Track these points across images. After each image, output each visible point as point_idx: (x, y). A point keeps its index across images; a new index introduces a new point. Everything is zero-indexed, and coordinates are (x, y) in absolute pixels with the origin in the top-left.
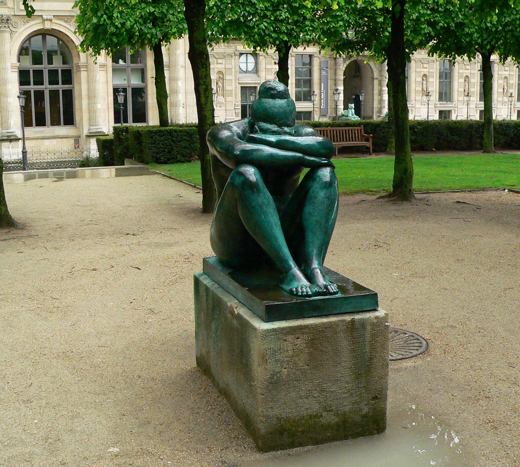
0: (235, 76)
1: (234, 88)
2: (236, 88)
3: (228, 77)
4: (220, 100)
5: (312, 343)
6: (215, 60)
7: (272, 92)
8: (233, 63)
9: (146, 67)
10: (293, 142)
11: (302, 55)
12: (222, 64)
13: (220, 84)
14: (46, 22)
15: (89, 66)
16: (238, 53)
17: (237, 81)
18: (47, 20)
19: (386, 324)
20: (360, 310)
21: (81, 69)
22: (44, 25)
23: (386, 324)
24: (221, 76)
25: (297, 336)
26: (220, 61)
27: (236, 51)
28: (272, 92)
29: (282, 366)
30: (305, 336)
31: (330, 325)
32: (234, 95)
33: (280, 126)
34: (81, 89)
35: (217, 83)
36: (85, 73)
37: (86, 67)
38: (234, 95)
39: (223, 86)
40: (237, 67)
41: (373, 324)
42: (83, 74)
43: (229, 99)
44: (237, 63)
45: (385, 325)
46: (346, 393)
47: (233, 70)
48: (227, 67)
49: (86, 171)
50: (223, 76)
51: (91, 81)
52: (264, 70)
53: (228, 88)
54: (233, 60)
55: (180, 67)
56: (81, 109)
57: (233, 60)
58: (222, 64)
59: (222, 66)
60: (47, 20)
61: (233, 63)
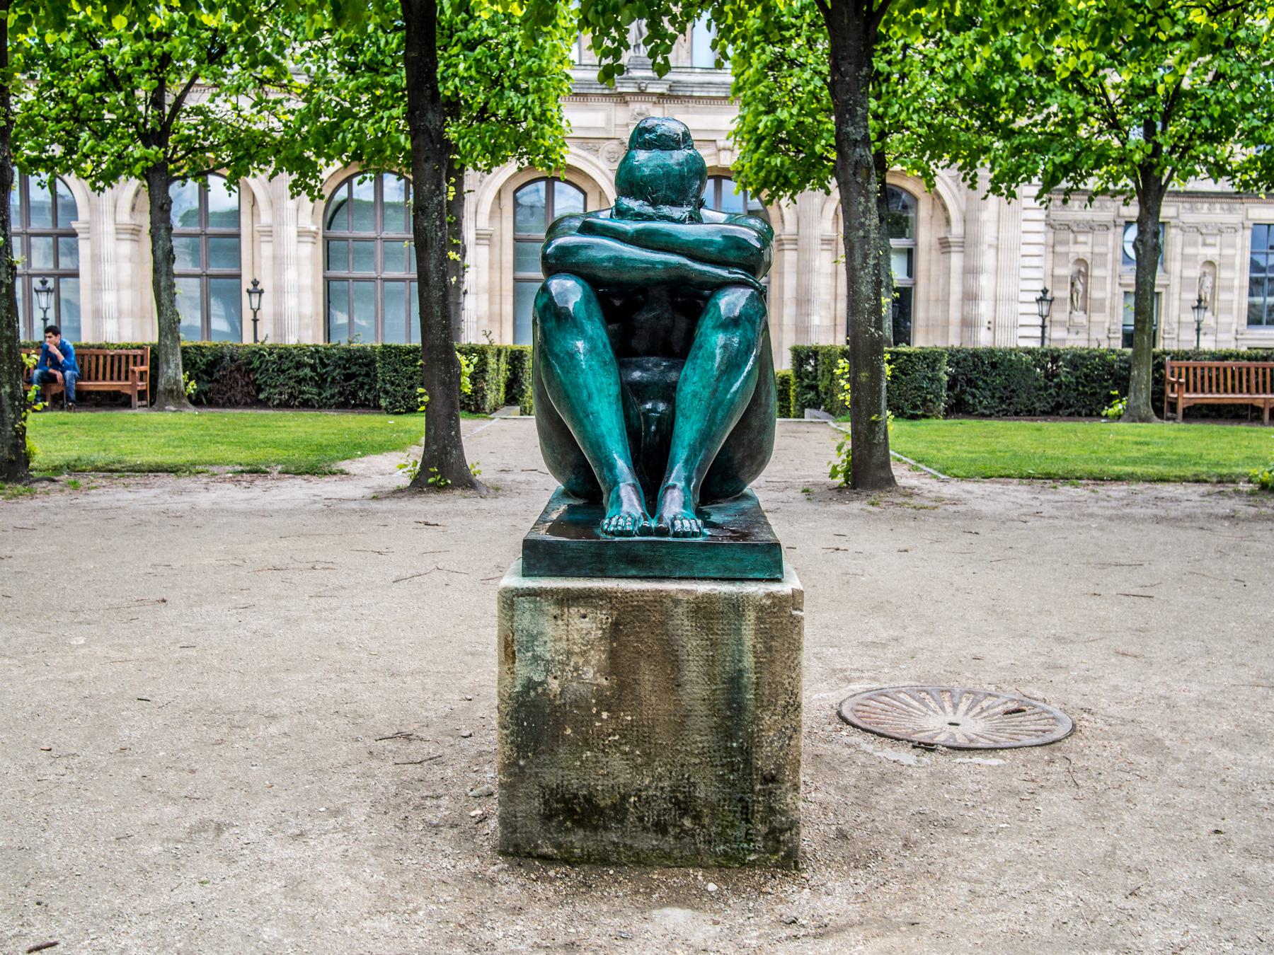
0: (1114, 270)
1: (1109, 295)
2: (1113, 294)
3: (1096, 272)
4: (1076, 320)
5: (615, 630)
6: (1072, 236)
7: (647, 136)
8: (1110, 243)
9: (916, 245)
10: (669, 235)
11: (1269, 225)
12: (1085, 243)
13: (1079, 286)
14: (723, 154)
15: (800, 243)
16: (1122, 221)
17: (1117, 280)
18: (724, 149)
19: (795, 613)
20: (738, 575)
21: (786, 247)
22: (719, 159)
23: (795, 613)
24: (1083, 269)
25: (582, 611)
26: (1081, 238)
27: (1119, 216)
28: (647, 136)
29: (547, 671)
30: (602, 615)
31: (659, 598)
32: (1108, 310)
33: (654, 204)
34: (781, 288)
35: (1073, 284)
36: (794, 254)
37: (795, 241)
38: (1108, 310)
39: (1086, 291)
40: (1119, 252)
41: (761, 609)
42: (790, 257)
43: (1096, 317)
44: (1120, 243)
45: (791, 615)
46: (696, 756)
47: (1110, 257)
48: (1097, 250)
49: (372, 308)
50: (1087, 270)
51: (804, 270)
52: (1179, 257)
53: (1095, 294)
54: (1111, 237)
55: (985, 247)
56: (781, 325)
57: (1111, 237)
58: (1085, 243)
59: (1087, 249)
60: (724, 149)
61: (1110, 243)
